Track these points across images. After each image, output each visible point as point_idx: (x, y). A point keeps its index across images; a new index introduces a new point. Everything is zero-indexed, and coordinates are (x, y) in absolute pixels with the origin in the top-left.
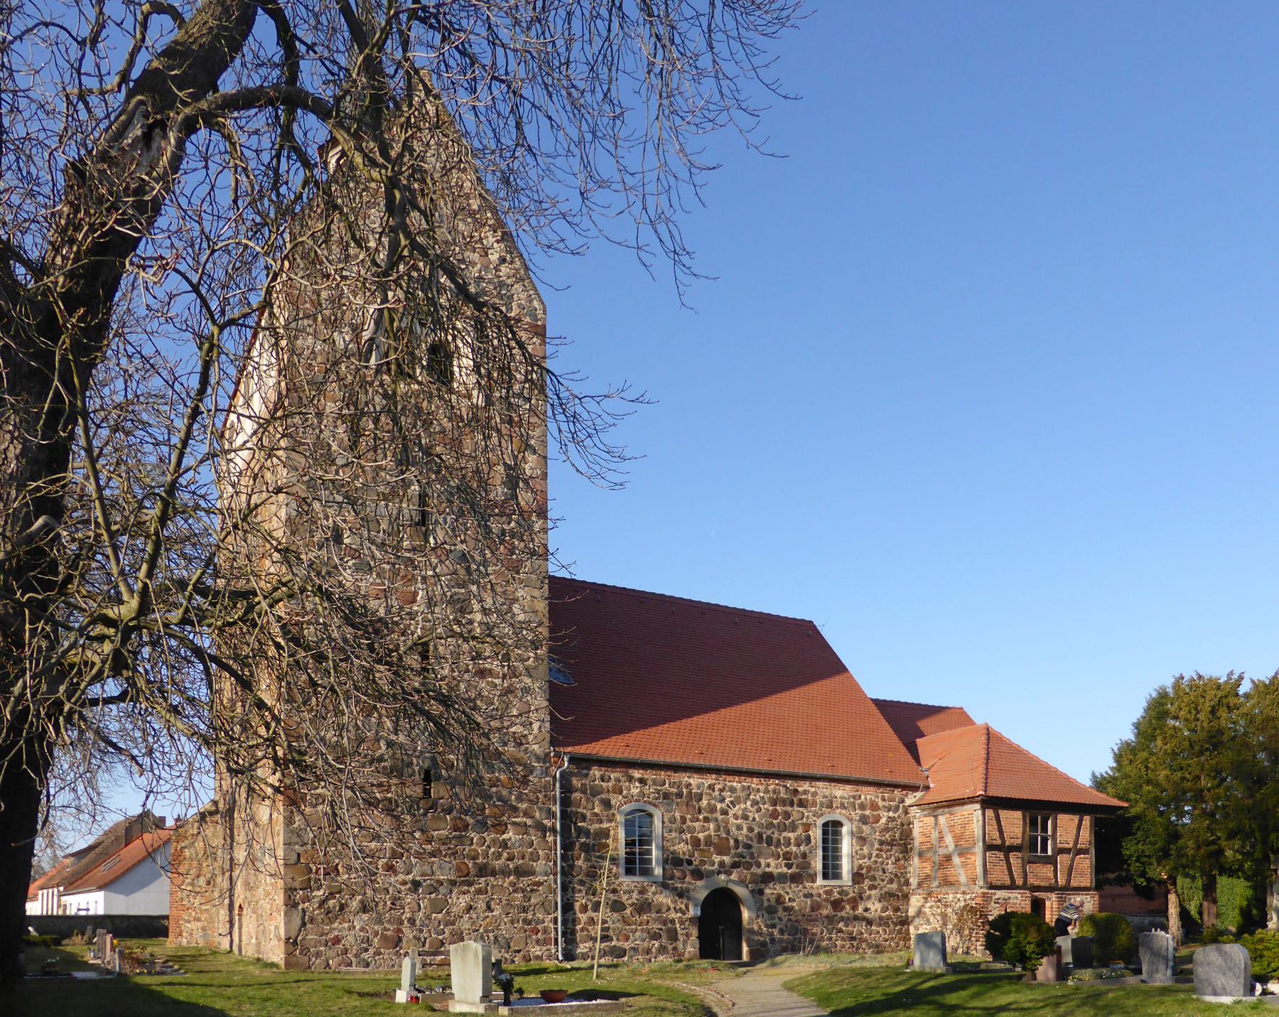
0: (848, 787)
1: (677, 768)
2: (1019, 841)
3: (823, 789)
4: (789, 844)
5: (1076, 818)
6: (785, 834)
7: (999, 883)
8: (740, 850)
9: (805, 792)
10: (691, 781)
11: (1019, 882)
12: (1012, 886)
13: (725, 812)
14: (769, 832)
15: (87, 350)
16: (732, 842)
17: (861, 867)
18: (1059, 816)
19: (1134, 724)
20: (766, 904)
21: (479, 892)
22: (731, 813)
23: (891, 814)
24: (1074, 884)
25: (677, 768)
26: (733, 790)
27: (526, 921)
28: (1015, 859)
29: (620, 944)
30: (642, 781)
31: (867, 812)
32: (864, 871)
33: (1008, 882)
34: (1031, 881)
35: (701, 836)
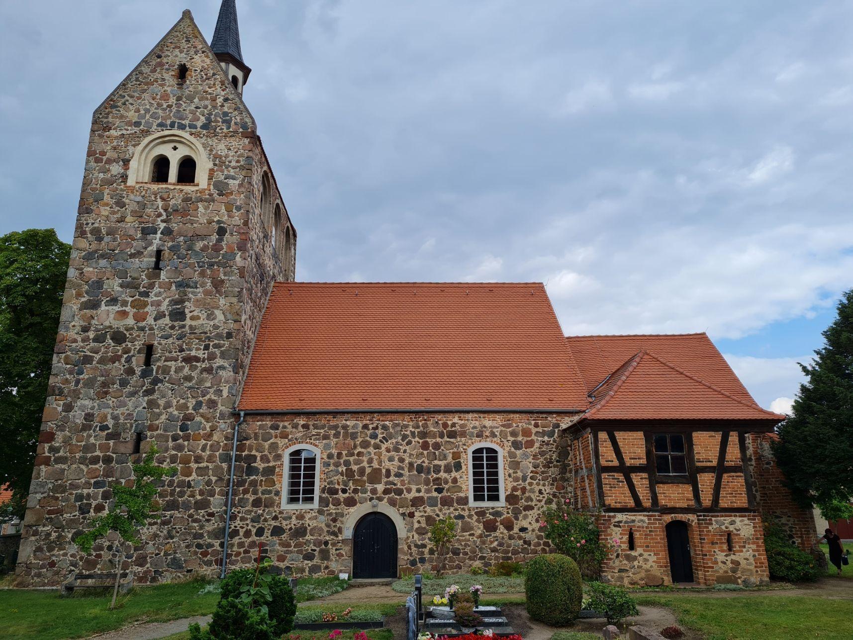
0: (498, 417)
1: (335, 414)
2: (644, 461)
3: (472, 422)
4: (439, 471)
5: (718, 436)
6: (436, 462)
7: (618, 506)
8: (391, 479)
9: (454, 425)
10: (348, 423)
11: (647, 503)
12: (638, 507)
13: (377, 447)
14: (419, 462)
15: (124, 85)
16: (384, 471)
17: (514, 489)
18: (695, 434)
19: (825, 334)
20: (416, 525)
21: (164, 523)
22: (384, 447)
23: (546, 439)
24: (723, 504)
25: (335, 414)
26: (385, 427)
27: (199, 546)
28: (641, 481)
29: (277, 564)
30: (305, 426)
31: (520, 438)
32: (518, 493)
33: (631, 503)
34: (663, 501)
35: (355, 468)
